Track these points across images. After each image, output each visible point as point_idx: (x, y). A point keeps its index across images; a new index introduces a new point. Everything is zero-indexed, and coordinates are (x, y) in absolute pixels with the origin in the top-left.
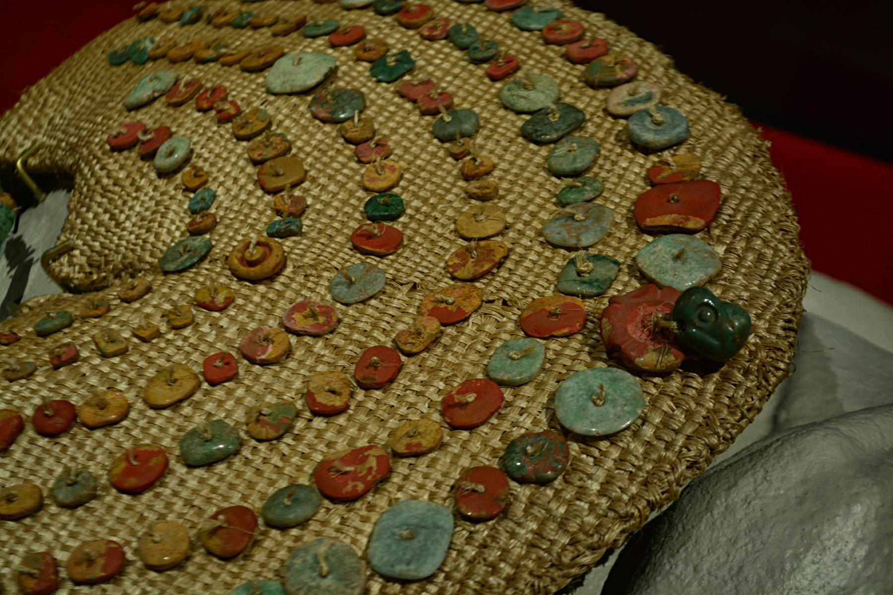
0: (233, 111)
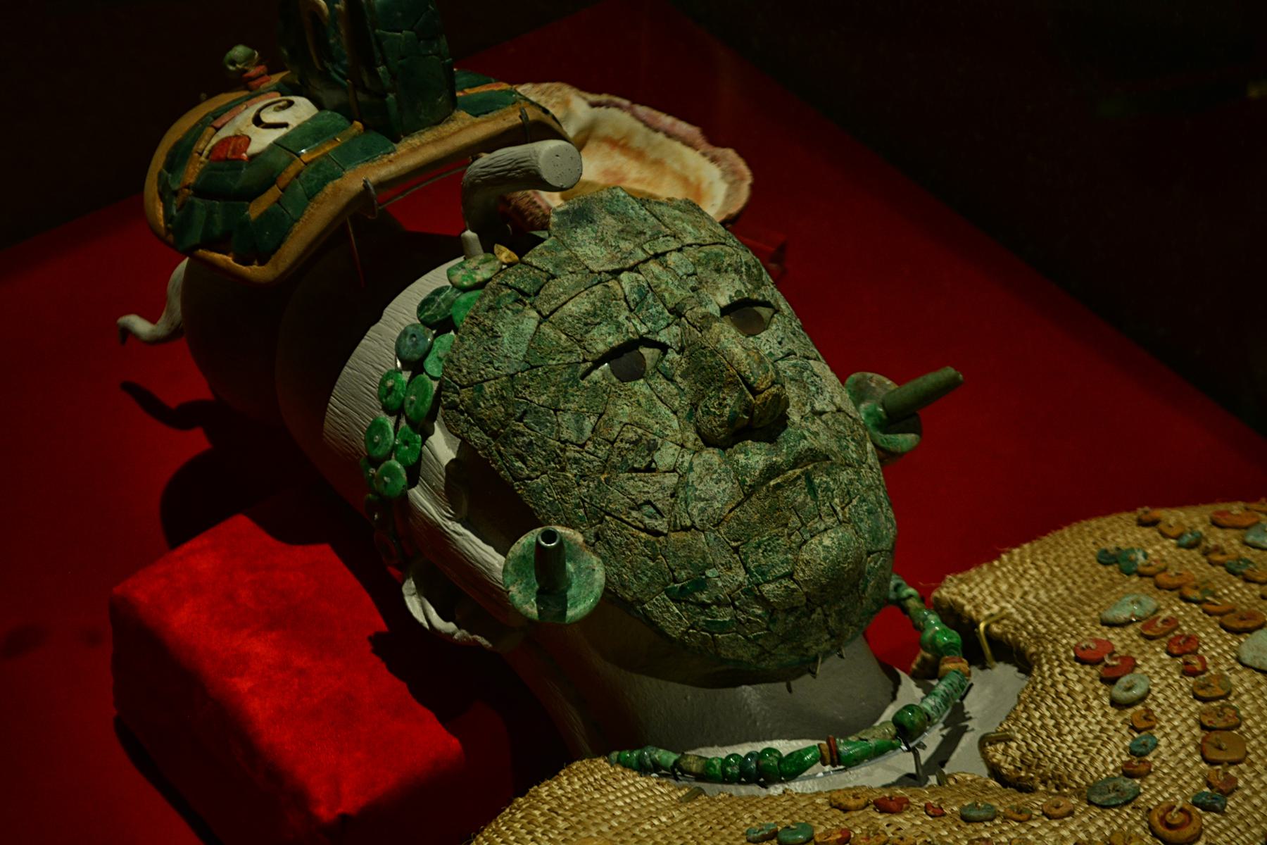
0: (1199, 668)
